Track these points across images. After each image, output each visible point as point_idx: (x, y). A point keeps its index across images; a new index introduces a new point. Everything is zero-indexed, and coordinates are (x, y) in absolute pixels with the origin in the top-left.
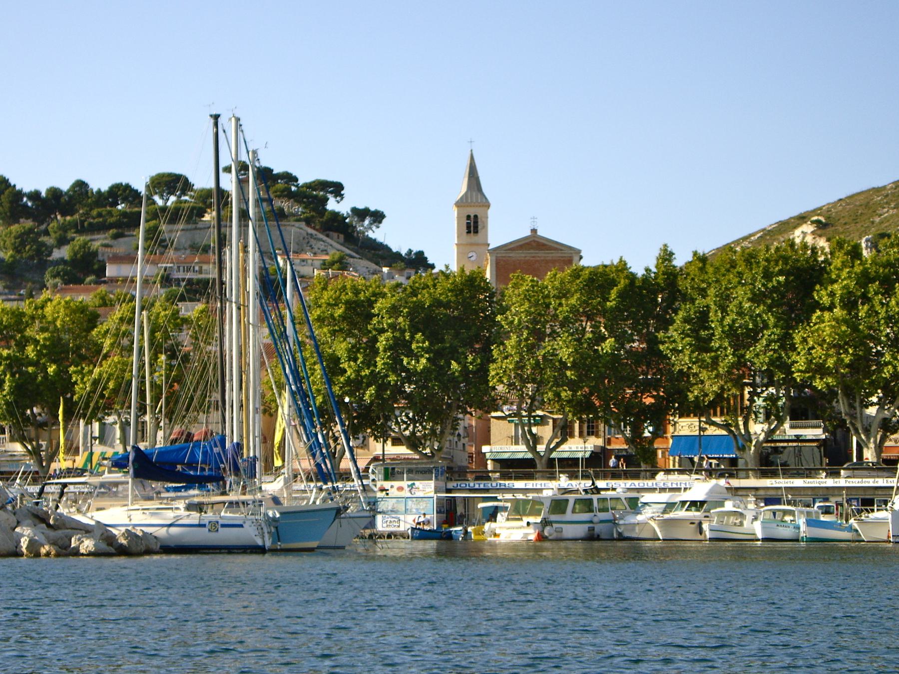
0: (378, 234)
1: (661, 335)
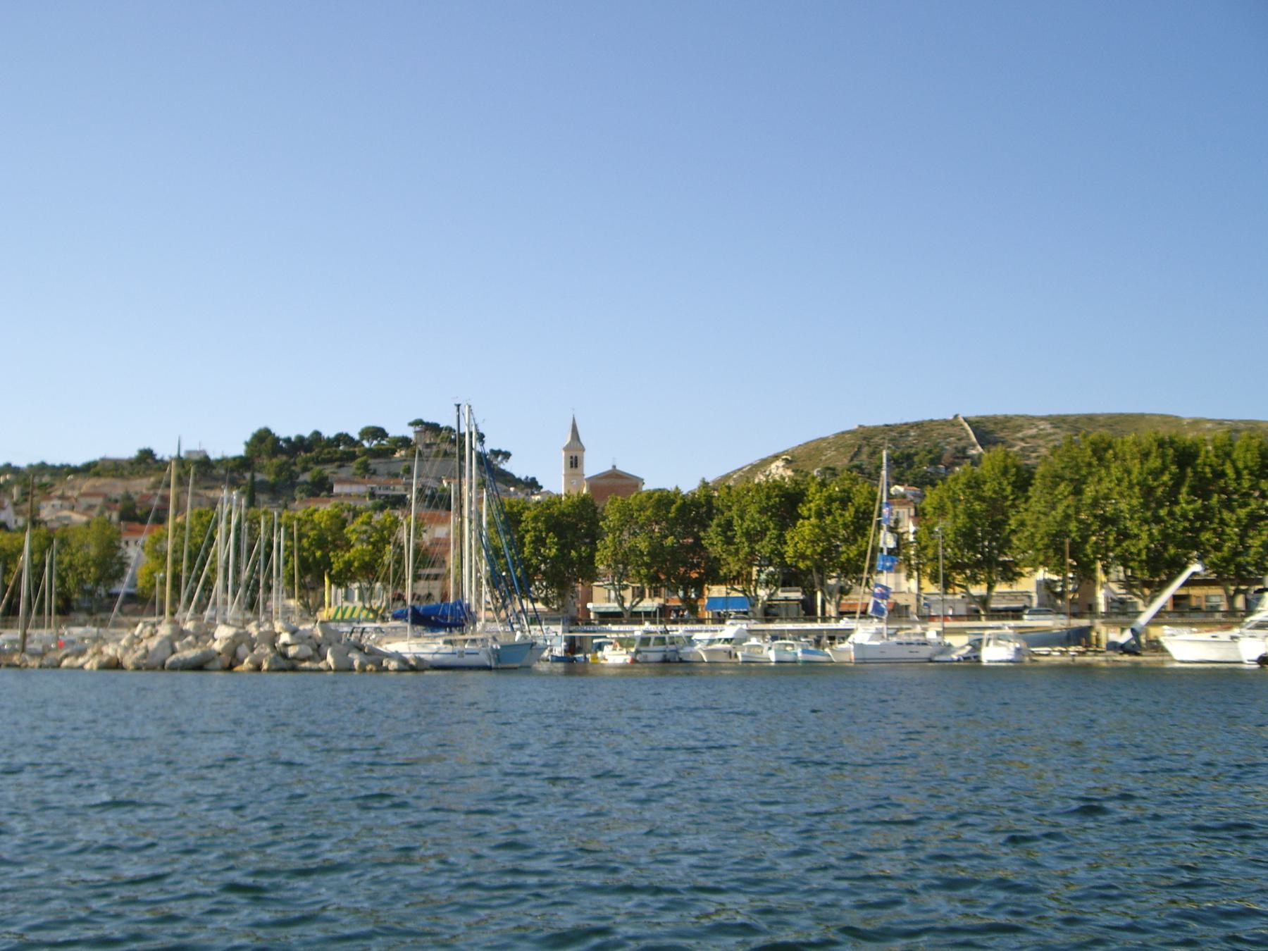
0: (506, 466)
1: (702, 534)
